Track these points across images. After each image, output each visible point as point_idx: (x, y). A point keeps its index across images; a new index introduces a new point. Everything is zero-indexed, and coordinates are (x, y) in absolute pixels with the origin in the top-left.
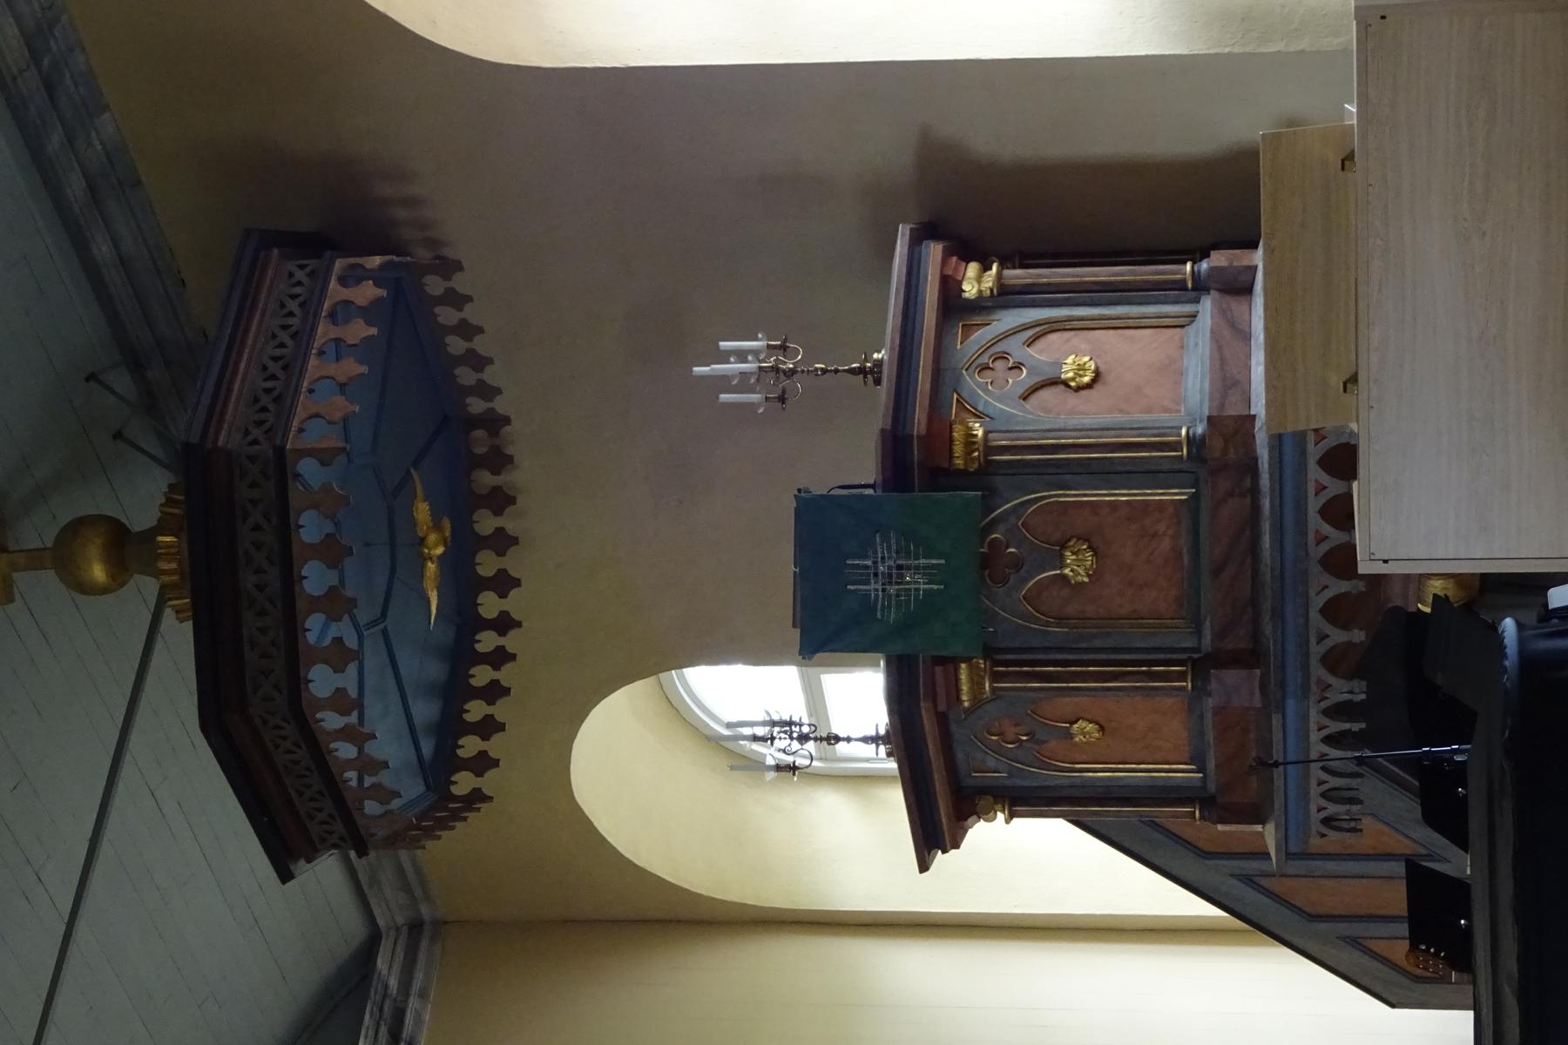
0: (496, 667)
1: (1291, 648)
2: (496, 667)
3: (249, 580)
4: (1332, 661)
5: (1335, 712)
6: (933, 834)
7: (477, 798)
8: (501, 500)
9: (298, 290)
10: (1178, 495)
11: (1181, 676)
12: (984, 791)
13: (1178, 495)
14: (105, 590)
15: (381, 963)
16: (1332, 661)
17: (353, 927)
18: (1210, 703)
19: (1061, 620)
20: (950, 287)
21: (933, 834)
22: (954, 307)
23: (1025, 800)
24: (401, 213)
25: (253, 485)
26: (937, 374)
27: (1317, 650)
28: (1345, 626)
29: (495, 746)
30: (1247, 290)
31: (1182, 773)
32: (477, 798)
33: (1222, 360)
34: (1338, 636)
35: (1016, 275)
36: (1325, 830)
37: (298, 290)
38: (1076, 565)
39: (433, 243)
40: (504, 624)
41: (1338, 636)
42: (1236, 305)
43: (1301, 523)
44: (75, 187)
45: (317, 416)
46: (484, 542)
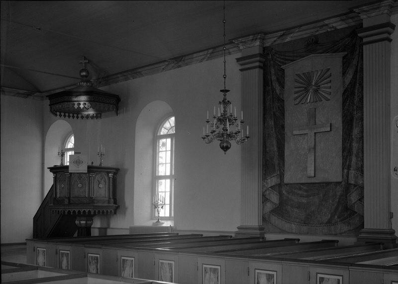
5: (64, 211)
6: (52, 169)
7: (56, 115)
8: (69, 117)
10: (87, 196)
12: (57, 175)
13: (87, 196)
14: (80, 75)
20: (110, 172)
21: (52, 169)
22: (108, 173)
23: (55, 179)
24: (122, 110)
29: (71, 118)
30: (109, 203)
31: (58, 196)
32: (56, 115)
34: (82, 212)
35: (111, 179)
38: (80, 185)
41: (82, 212)
44: (125, 74)
45: (331, 131)
46: (77, 115)
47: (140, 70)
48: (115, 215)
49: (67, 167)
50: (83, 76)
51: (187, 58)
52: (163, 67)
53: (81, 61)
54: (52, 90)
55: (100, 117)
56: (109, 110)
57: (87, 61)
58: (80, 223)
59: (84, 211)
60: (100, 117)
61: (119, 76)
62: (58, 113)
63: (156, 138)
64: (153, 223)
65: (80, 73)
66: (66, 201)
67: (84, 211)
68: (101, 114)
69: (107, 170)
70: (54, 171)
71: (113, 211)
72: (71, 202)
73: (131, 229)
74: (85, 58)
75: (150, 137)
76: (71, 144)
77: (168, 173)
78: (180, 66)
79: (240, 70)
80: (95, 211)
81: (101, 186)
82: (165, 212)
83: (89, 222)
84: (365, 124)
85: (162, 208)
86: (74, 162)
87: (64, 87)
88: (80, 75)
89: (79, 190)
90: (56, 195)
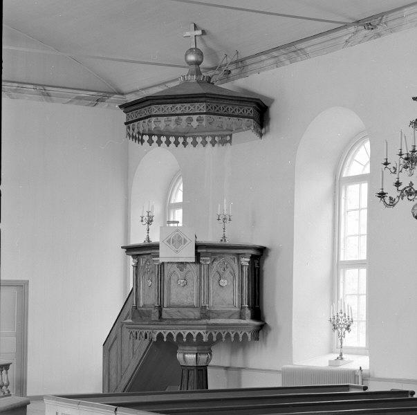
0: (174, 143)
1: (163, 326)
2: (174, 143)
3: (179, 106)
4: (170, 335)
7: (142, 141)
9: (245, 111)
11: (158, 304)
14: (186, 58)
15: (116, 96)
16: (170, 335)
17: (124, 90)
18: (152, 309)
19: (170, 279)
25: (198, 107)
26: (223, 253)
27: (162, 332)
28: (186, 338)
30: (241, 318)
31: (141, 303)
32: (142, 141)
33: (224, 313)
35: (245, 269)
36: (208, 333)
37: (245, 111)
39: (265, 133)
40: (185, 144)
42: (237, 316)
43: (187, 329)
44: (275, 54)
47: (299, 46)
48: (258, 344)
49: (156, 247)
50: (190, 63)
51: (391, 16)
52: (347, 38)
53: (188, 34)
54: (143, 89)
55: (230, 141)
56: (239, 129)
57: (199, 32)
58: (184, 358)
59: (189, 334)
60: (230, 141)
61: (263, 57)
62: (146, 138)
63: (338, 184)
64: (330, 361)
65: (186, 55)
66: (155, 316)
67: (189, 334)
68: (231, 136)
69: (235, 250)
70: (135, 253)
71: (249, 335)
72: (164, 315)
73: (286, 374)
74: (196, 28)
75: (326, 183)
76: (178, 197)
77: (364, 257)
78: (379, 35)
79: (185, 147)
80: (211, 334)
81: (224, 282)
82: (356, 337)
83: (203, 357)
84: (168, 261)
85: (348, 328)
86: (169, 241)
87: (164, 83)
88: (186, 58)
89: (182, 293)
90: (137, 300)
